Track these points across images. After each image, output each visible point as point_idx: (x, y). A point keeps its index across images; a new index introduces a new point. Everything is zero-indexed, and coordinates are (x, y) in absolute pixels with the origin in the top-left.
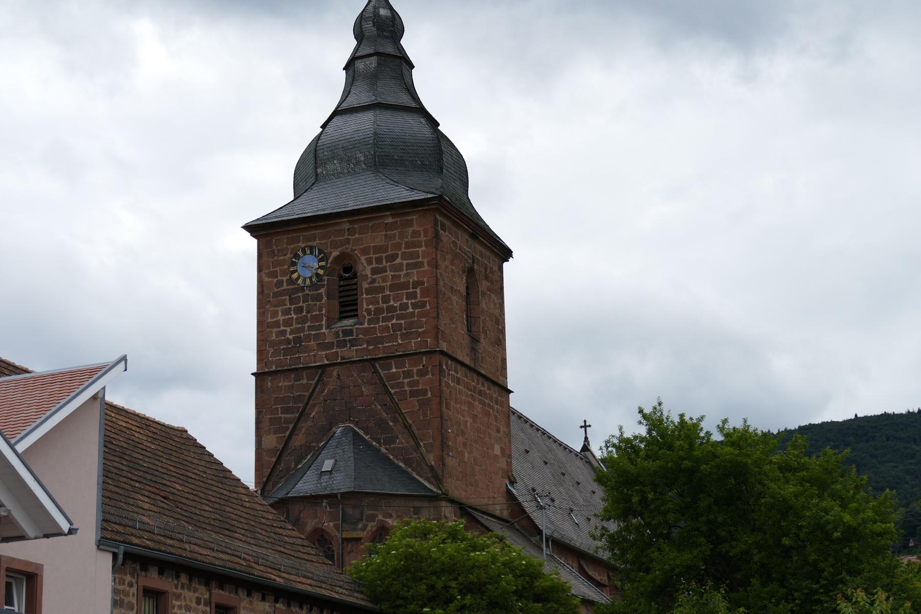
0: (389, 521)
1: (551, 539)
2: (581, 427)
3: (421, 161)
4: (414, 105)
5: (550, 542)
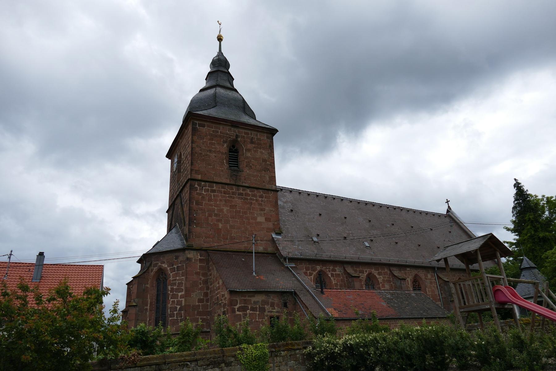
0: (163, 265)
1: (287, 258)
2: (446, 203)
3: (207, 104)
4: (231, 87)
5: (287, 260)
